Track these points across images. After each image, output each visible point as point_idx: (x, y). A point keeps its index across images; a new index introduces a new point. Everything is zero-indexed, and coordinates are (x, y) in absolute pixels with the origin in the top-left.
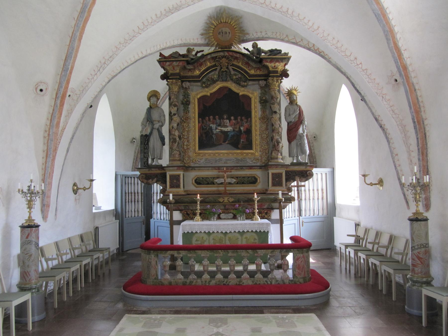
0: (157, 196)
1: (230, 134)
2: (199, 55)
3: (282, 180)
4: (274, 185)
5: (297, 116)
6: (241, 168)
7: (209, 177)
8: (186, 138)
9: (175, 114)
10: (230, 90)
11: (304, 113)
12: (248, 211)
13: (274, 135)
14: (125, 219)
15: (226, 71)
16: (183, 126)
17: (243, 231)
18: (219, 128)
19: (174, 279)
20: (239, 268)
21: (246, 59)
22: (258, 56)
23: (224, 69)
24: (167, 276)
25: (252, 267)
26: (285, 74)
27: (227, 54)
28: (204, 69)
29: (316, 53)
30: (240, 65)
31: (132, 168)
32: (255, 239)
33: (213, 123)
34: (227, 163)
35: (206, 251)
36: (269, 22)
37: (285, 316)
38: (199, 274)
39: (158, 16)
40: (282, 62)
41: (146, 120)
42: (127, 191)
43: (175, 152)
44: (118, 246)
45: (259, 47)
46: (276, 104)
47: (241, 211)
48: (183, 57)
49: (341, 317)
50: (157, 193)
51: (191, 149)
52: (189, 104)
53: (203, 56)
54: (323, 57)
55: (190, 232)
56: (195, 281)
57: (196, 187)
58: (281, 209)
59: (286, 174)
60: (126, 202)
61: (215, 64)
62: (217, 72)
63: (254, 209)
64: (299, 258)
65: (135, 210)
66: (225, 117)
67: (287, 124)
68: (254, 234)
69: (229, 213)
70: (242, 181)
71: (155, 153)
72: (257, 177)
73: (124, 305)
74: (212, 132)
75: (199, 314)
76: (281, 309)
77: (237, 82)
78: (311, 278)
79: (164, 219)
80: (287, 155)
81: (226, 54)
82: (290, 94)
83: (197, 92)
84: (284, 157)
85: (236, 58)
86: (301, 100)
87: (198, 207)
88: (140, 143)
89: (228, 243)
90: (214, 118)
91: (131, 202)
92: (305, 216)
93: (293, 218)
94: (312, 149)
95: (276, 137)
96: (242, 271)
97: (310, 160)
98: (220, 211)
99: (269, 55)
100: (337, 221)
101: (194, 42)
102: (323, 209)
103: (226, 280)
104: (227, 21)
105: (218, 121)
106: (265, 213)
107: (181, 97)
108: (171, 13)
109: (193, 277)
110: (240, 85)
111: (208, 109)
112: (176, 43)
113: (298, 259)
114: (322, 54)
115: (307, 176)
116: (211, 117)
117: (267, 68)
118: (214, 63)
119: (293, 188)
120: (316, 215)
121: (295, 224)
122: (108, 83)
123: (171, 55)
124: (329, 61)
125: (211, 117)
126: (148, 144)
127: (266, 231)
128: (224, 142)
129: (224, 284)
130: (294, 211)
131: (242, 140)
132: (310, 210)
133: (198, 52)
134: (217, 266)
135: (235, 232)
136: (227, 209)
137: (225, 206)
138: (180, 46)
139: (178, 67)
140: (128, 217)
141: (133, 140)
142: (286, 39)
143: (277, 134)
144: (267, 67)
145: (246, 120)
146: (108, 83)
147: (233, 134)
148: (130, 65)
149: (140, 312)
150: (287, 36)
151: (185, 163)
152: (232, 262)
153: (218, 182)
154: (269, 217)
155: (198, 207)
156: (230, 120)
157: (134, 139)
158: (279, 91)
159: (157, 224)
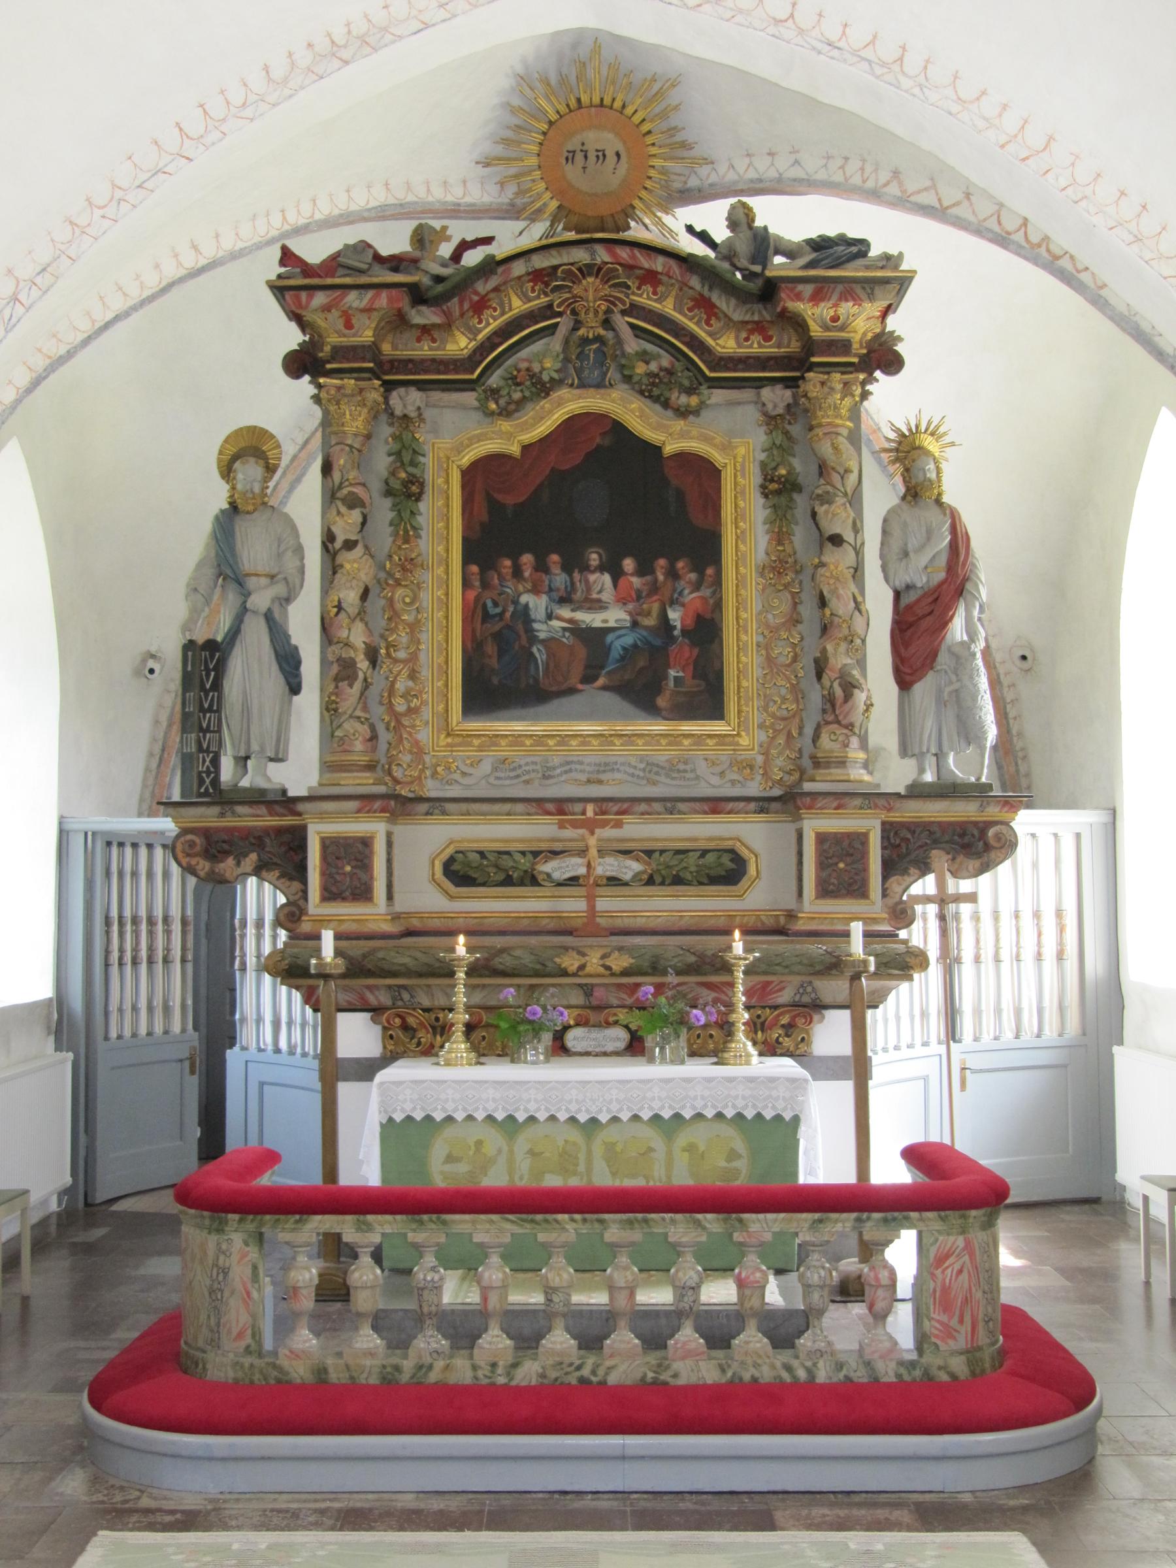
0: (259, 937)
1: (619, 644)
2: (472, 258)
3: (865, 869)
4: (825, 891)
5: (943, 561)
6: (671, 805)
7: (511, 847)
8: (405, 662)
9: (349, 545)
10: (618, 429)
11: (974, 544)
12: (698, 1016)
13: (829, 647)
14: (101, 1045)
15: (599, 339)
16: (391, 601)
17: (677, 1116)
18: (566, 612)
19: (339, 1355)
20: (657, 1296)
21: (695, 282)
22: (757, 268)
23: (592, 328)
24: (305, 1339)
25: (720, 1293)
26: (883, 357)
27: (607, 259)
28: (494, 325)
29: (1035, 260)
30: (668, 307)
31: (142, 800)
32: (733, 1155)
33: (536, 590)
34: (600, 782)
35: (494, 1217)
36: (811, 106)
37: (880, 1541)
38: (463, 1330)
39: (278, 73)
40: (871, 297)
41: (210, 572)
42: (114, 913)
43: (350, 726)
44: (68, 1180)
45: (758, 223)
46: (840, 500)
47: (665, 1019)
48: (396, 270)
49: (1156, 1553)
50: (260, 924)
51: (427, 713)
52: (418, 497)
53: (490, 266)
54: (1068, 278)
55: (418, 1116)
56: (440, 1364)
57: (452, 898)
58: (859, 1007)
59: (885, 837)
60: (107, 965)
61: (550, 306)
62: (555, 343)
63: (730, 1006)
64: (947, 1256)
65: (152, 1002)
66: (594, 559)
67: (890, 595)
68: (729, 1131)
69: (608, 1024)
70: (670, 870)
71: (254, 729)
72: (745, 853)
73: (95, 1481)
74: (530, 631)
75: (460, 1529)
76: (859, 1505)
77: (654, 391)
78: (1003, 1353)
79: (292, 1052)
80: (891, 742)
81: (602, 255)
82: (907, 452)
83: (459, 436)
84: (879, 750)
85: (651, 278)
86: (958, 484)
87: (460, 997)
88: (177, 675)
89: (603, 1178)
90: (542, 567)
91: (135, 962)
92: (976, 1039)
93: (919, 1050)
94: (1012, 714)
95: (840, 659)
96: (667, 1314)
97: (1000, 767)
98: (568, 1017)
99: (807, 266)
100: (1130, 1068)
101: (449, 198)
102: (1061, 1008)
103: (590, 1361)
104: (607, 101)
105: (560, 579)
106: (783, 1030)
107: (382, 462)
108: (336, 63)
109: (429, 1343)
110: (666, 405)
111: (516, 519)
112: (361, 200)
113: (941, 1260)
114: (1065, 263)
115: (987, 847)
116: (527, 559)
117: (799, 326)
118: (544, 300)
119: (919, 908)
120: (1027, 1037)
121: (926, 1079)
122: (29, 390)
123: (334, 258)
124: (1098, 300)
125: (527, 559)
126: (217, 686)
127: (787, 1116)
128: (588, 679)
129: (582, 1380)
130: (924, 1014)
131: (672, 673)
132: (998, 1011)
133: (464, 246)
134: (549, 1291)
135: (636, 1118)
136: (599, 1008)
137: (588, 990)
138: (383, 214)
139: (370, 319)
140: (120, 1037)
141: (144, 661)
142: (893, 190)
143: (843, 646)
144: (798, 324)
145: (693, 576)
146: (29, 390)
147: (628, 640)
148: (135, 308)
149: (168, 1518)
150: (896, 173)
151: (397, 781)
152: (623, 1271)
153: (557, 875)
154: (803, 1048)
155: (460, 997)
156: (617, 574)
157: (153, 656)
158: (855, 438)
159: (257, 1074)
